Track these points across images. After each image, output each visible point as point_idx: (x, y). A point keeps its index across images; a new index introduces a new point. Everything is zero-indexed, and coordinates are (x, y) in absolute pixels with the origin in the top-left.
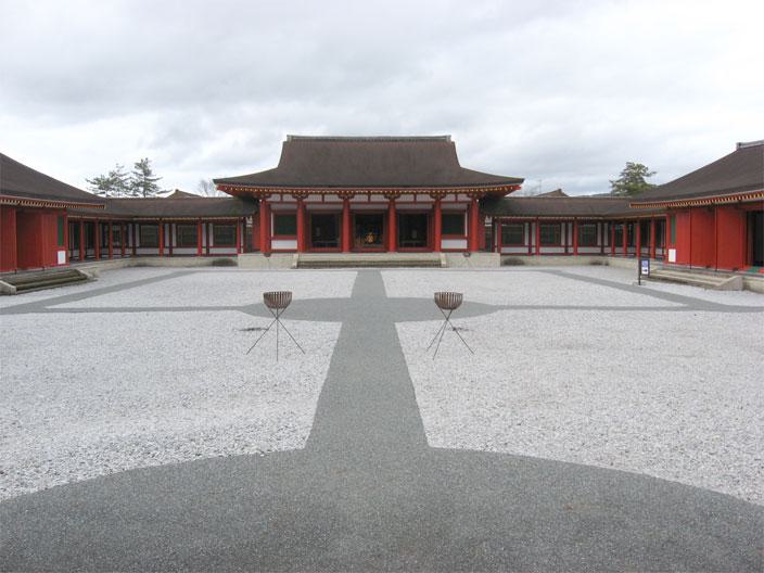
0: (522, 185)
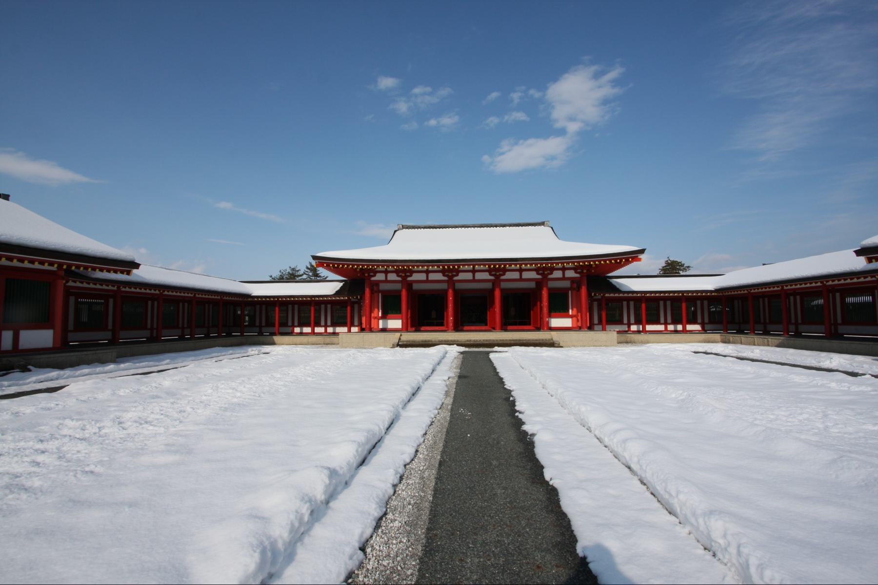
0: (135, 271)
